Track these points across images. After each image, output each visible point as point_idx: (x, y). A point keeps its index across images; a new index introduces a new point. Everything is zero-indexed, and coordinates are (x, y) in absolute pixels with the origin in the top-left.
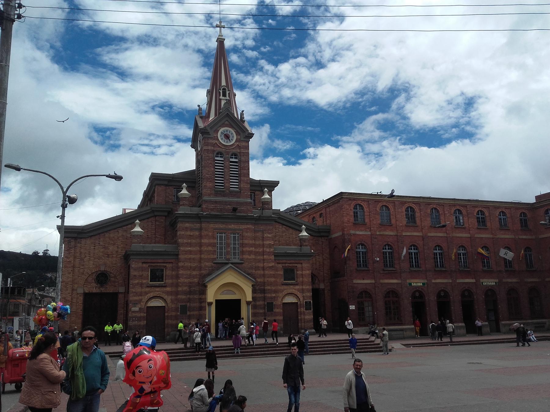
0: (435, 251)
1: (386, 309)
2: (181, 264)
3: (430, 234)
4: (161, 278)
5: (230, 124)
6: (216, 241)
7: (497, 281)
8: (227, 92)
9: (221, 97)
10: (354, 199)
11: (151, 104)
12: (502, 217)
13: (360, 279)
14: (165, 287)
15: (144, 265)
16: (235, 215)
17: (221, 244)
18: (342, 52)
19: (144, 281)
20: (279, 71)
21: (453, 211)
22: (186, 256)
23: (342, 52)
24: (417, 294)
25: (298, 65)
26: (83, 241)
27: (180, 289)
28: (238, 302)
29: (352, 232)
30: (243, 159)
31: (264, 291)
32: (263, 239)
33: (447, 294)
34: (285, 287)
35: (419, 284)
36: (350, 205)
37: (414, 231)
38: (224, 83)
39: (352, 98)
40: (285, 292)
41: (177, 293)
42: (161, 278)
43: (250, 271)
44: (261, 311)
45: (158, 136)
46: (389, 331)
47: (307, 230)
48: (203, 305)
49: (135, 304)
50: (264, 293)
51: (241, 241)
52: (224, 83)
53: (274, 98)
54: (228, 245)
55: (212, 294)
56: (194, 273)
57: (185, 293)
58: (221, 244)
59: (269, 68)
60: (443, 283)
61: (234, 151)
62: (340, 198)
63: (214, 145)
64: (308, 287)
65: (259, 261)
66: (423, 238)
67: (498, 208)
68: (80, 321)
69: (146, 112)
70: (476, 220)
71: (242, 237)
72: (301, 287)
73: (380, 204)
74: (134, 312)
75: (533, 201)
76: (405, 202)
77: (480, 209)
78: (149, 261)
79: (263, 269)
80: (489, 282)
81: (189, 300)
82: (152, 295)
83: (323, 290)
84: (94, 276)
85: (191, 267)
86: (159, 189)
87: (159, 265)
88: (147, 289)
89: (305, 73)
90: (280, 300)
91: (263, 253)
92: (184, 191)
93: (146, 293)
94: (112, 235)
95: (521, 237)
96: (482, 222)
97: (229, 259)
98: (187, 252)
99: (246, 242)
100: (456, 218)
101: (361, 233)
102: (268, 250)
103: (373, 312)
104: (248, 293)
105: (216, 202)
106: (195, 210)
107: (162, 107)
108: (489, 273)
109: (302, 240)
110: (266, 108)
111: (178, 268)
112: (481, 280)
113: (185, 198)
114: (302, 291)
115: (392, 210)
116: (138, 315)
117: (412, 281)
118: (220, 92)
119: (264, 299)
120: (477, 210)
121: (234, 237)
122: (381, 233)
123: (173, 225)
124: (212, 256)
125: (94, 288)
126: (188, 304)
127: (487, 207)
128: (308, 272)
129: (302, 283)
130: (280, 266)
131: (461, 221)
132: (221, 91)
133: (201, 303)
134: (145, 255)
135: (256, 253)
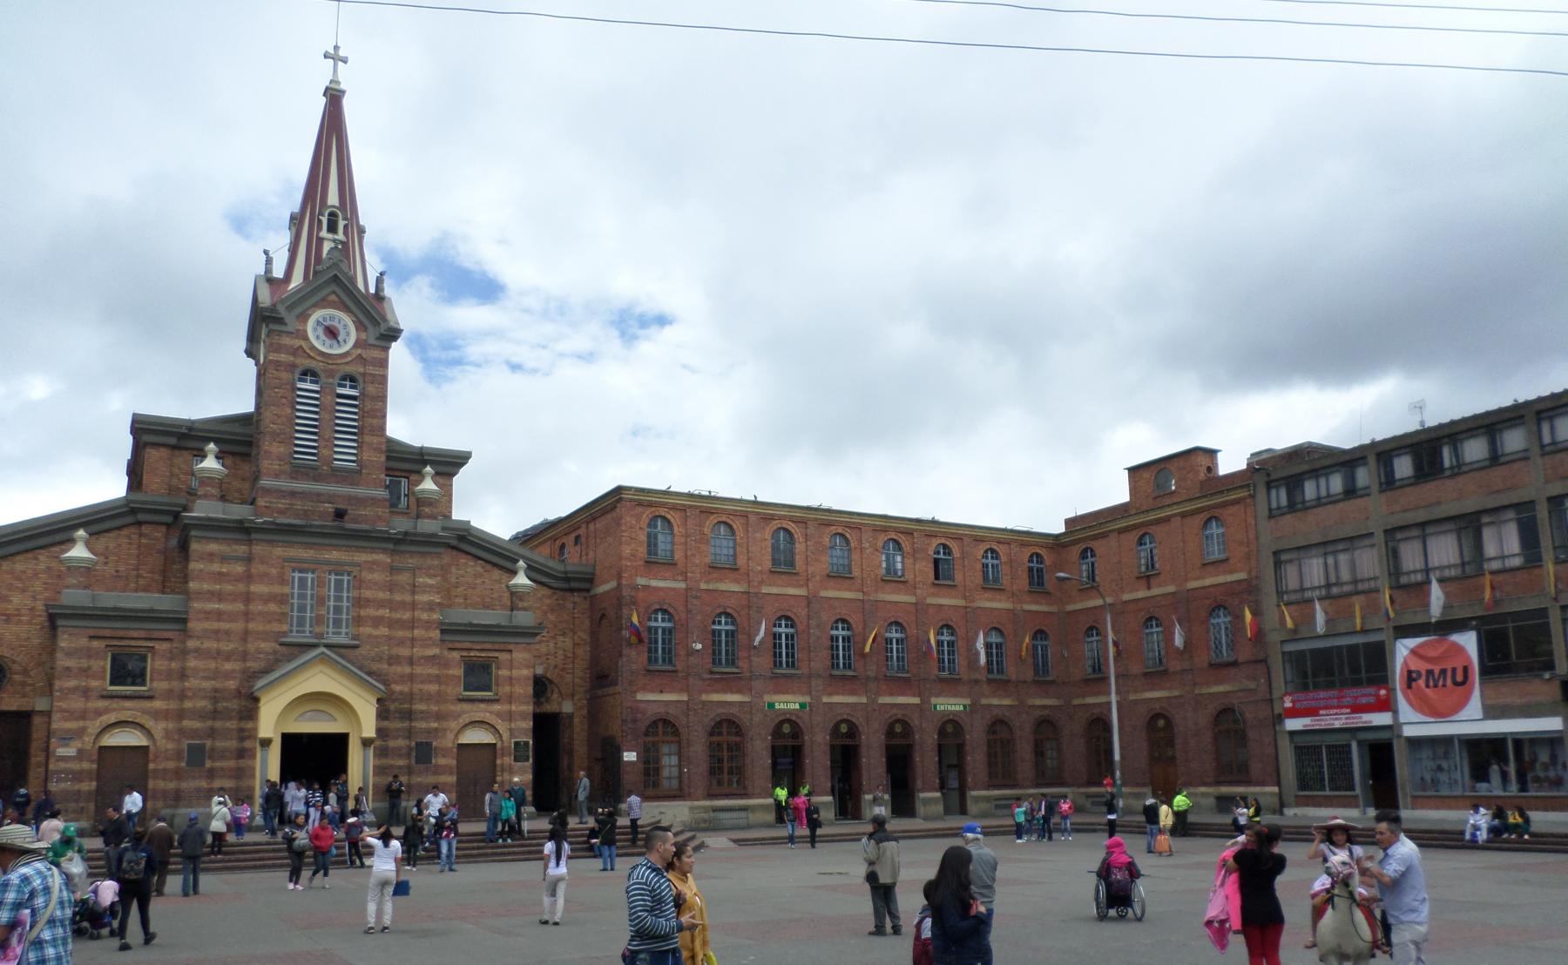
0: (834, 632)
2: (191, 644)
3: (824, 594)
4: (138, 677)
5: (343, 303)
6: (286, 590)
7: (968, 701)
8: (341, 224)
9: (324, 233)
10: (651, 505)
12: (990, 561)
13: (652, 691)
14: (151, 698)
15: (95, 644)
16: (340, 528)
17: (302, 596)
19: (94, 683)
21: (880, 544)
22: (208, 625)
27: (188, 704)
28: (341, 741)
29: (641, 581)
30: (371, 389)
31: (409, 715)
32: (414, 589)
33: (853, 731)
34: (466, 706)
36: (638, 517)
38: (333, 198)
41: (180, 715)
42: (138, 677)
43: (375, 667)
47: (532, 570)
48: (248, 744)
49: (67, 738)
50: (411, 720)
51: (355, 593)
52: (333, 198)
54: (321, 601)
55: (273, 718)
56: (228, 666)
57: (201, 715)
58: (302, 596)
62: (614, 501)
63: (296, 351)
64: (523, 708)
66: (808, 601)
71: (359, 583)
72: (506, 707)
78: (107, 633)
79: (411, 661)
80: (949, 704)
81: (212, 733)
82: (112, 718)
83: (571, 716)
85: (219, 652)
86: (153, 455)
87: (133, 643)
88: (102, 704)
90: (450, 736)
91: (412, 624)
92: (210, 463)
93: (99, 713)
95: (1027, 607)
96: (940, 570)
97: (320, 636)
98: (208, 615)
99: (368, 594)
100: (888, 556)
101: (661, 584)
102: (425, 616)
103: (680, 766)
106: (237, 511)
108: (951, 684)
109: (515, 595)
111: (185, 652)
112: (934, 700)
114: (509, 717)
115: (740, 533)
116: (75, 766)
118: (320, 222)
119: (410, 733)
121: (339, 584)
122: (711, 587)
123: (184, 547)
124: (276, 627)
126: (209, 743)
129: (510, 699)
130: (456, 655)
131: (899, 566)
132: (325, 220)
133: (242, 739)
135: (392, 624)
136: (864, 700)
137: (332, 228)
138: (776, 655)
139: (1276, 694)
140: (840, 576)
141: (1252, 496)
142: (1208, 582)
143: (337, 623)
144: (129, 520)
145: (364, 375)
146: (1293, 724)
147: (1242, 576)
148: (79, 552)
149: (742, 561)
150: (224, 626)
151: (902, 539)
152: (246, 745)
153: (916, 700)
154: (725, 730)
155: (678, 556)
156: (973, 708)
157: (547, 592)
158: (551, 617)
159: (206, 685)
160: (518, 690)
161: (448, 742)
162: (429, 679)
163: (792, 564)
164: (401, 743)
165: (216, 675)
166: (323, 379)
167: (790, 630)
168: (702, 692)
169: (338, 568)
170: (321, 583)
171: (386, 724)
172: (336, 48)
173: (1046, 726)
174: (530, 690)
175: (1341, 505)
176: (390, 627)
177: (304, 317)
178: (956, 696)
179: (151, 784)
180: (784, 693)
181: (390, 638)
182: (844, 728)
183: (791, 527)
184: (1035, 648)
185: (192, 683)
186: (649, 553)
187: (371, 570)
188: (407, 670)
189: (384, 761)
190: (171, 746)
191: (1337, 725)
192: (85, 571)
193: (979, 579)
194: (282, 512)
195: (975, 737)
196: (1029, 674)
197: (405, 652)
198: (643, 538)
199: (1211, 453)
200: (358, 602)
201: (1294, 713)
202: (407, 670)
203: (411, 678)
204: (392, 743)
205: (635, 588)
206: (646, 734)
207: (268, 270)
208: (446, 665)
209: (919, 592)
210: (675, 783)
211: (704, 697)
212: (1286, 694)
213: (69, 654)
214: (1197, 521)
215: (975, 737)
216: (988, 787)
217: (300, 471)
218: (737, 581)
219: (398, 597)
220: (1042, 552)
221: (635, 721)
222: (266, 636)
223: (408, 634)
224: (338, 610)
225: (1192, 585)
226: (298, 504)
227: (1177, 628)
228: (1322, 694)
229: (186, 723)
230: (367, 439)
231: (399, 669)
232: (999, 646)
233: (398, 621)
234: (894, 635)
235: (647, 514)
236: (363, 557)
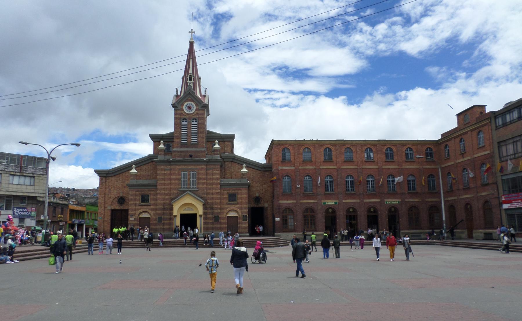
0: (347, 179)
1: (305, 220)
2: (158, 192)
3: (343, 167)
6: (180, 177)
7: (400, 200)
8: (193, 78)
9: (188, 81)
10: (283, 145)
11: (273, 67)
12: (409, 152)
13: (284, 200)
14: (150, 205)
15: (137, 193)
16: (192, 159)
17: (184, 178)
18: (432, 8)
19: (137, 202)
20: (376, 31)
21: (364, 150)
23: (432, 8)
24: (393, 209)
25: (394, 24)
26: (110, 178)
27: (158, 207)
28: (195, 216)
29: (280, 168)
30: (200, 122)
31: (212, 208)
32: (213, 174)
34: (229, 206)
35: (332, 203)
36: (279, 149)
37: (330, 165)
38: (191, 71)
39: (443, 45)
40: (229, 209)
43: (203, 196)
44: (211, 221)
45: (278, 92)
46: (316, 235)
48: (172, 217)
49: (132, 216)
51: (197, 177)
52: (191, 71)
53: (370, 52)
54: (189, 179)
55: (177, 210)
56: (167, 197)
57: (161, 210)
58: (184, 178)
59: (366, 28)
60: (352, 202)
61: (194, 117)
63: (181, 114)
64: (245, 206)
65: (210, 189)
66: (337, 170)
67: (405, 145)
68: (109, 226)
69: (268, 74)
70: (384, 155)
71: (198, 174)
73: (304, 147)
74: (131, 220)
75: (440, 138)
76: (324, 145)
77: (389, 146)
78: (140, 190)
79: (213, 194)
80: (393, 202)
81: (164, 214)
82: (141, 210)
83: (267, 208)
84: (117, 199)
85: (164, 194)
88: (139, 207)
89: (398, 29)
91: (212, 184)
93: (139, 209)
94: (127, 175)
95: (424, 167)
96: (390, 157)
97: (189, 188)
98: (161, 184)
99: (200, 176)
100: (367, 153)
101: (287, 168)
102: (216, 182)
103: (294, 223)
104: (199, 210)
105: (181, 152)
107: (280, 69)
108: (393, 195)
109: (244, 174)
110: (364, 61)
111: (157, 194)
112: (386, 200)
113: (161, 150)
114: (241, 208)
115: (313, 150)
116: (133, 222)
117: (326, 201)
119: (213, 213)
120: (386, 147)
121: (193, 174)
124: (178, 187)
125: (117, 207)
126: (163, 216)
127: (395, 145)
128: (245, 196)
129: (241, 203)
130: (226, 192)
131: (372, 156)
132: (188, 78)
133: (170, 215)
134: (136, 186)
136: (358, 201)
137: (190, 79)
138: (347, 187)
139: (500, 196)
140: (349, 161)
141: (490, 122)
142: (479, 155)
143: (193, 185)
144: (150, 161)
145: (198, 118)
146: (506, 206)
147: (488, 152)
148: (134, 171)
149: (313, 159)
150: (166, 187)
151: (372, 147)
152: (172, 217)
153: (379, 200)
154: (309, 211)
155: (292, 159)
156: (402, 203)
157: (259, 172)
158: (261, 179)
159: (162, 202)
160: (243, 201)
161: (224, 215)
162: (217, 199)
163: (331, 159)
164: (211, 216)
165: (164, 199)
166: (188, 120)
167: (331, 180)
168: (300, 200)
169: (193, 170)
170: (189, 174)
171: (206, 211)
172: (192, 30)
173: (413, 210)
174: (247, 201)
175: (517, 123)
176: (207, 185)
177: (182, 105)
178: (395, 199)
179: (151, 227)
180: (330, 199)
181: (206, 188)
182: (372, 210)
183: (331, 147)
184: (429, 181)
185: (159, 201)
186: (283, 159)
187: (201, 170)
188: (212, 196)
189: (206, 221)
190: (154, 217)
191: (518, 206)
192: (135, 175)
193: (404, 158)
194: (179, 157)
195: (403, 213)
196: (427, 190)
197: (211, 191)
198: (281, 154)
199: (484, 107)
200: (198, 179)
201: (506, 202)
202: (212, 196)
203: (213, 198)
204: (208, 216)
205: (278, 170)
206: (283, 213)
207: (177, 93)
208: (223, 195)
209: (379, 164)
210: (293, 227)
211: (301, 201)
212: (504, 195)
213: (132, 195)
214: (475, 133)
215: (403, 213)
216: (408, 230)
217: (183, 145)
218: (312, 165)
219: (209, 177)
220: (432, 147)
221: (279, 209)
222: (175, 189)
223: (211, 187)
224: (193, 181)
225: (475, 156)
226: (182, 154)
227: (319, 182)
228: (513, 195)
229: (157, 212)
230: (199, 135)
231: (210, 196)
232: (413, 181)
233: (209, 183)
234: (370, 179)
235: (282, 147)
236: (198, 167)
